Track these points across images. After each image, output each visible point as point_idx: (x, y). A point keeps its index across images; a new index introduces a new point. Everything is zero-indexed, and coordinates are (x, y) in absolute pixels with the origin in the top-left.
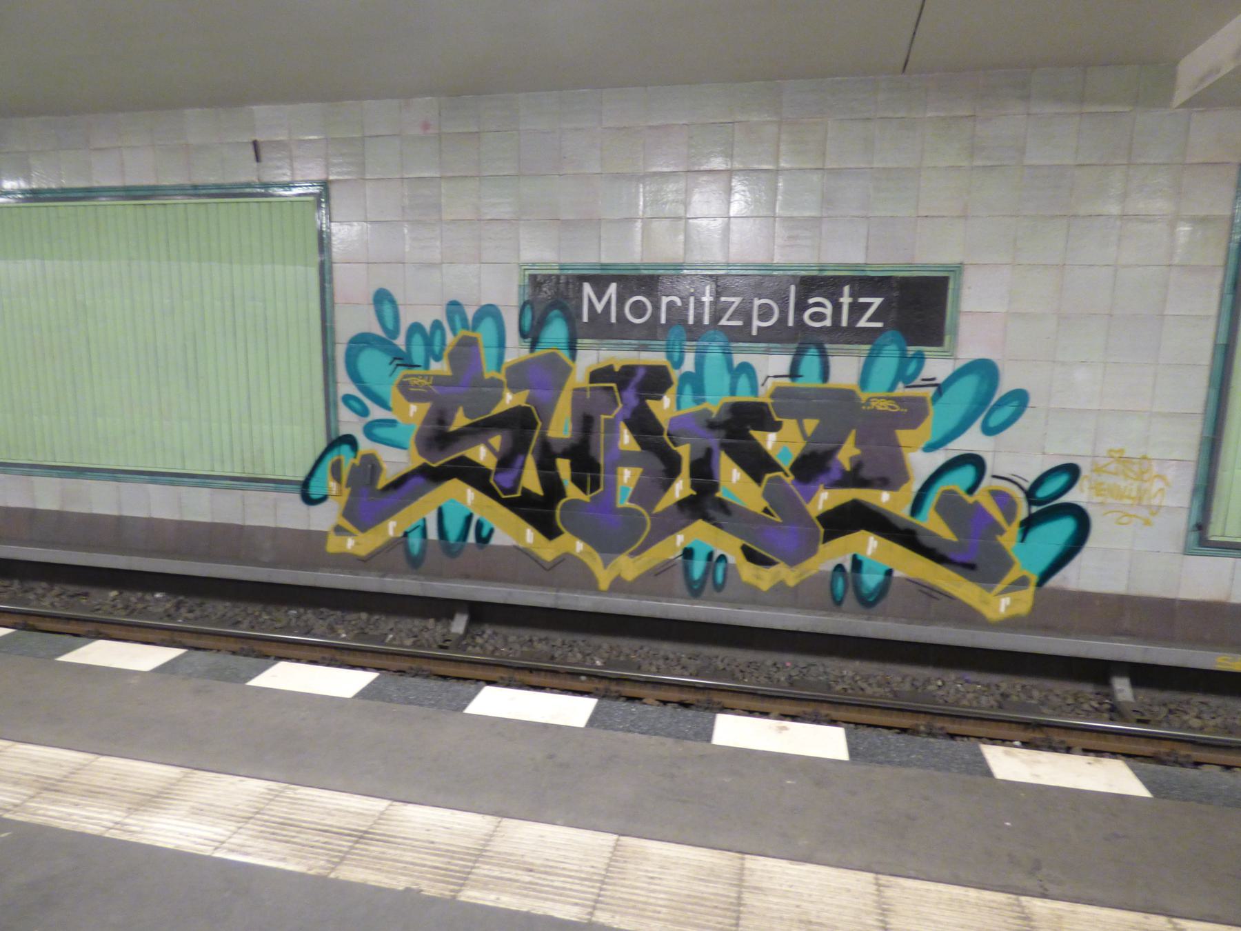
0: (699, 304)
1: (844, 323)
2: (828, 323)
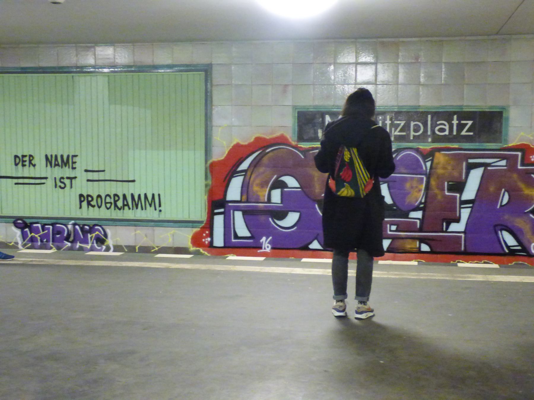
1: (455, 133)
2: (447, 133)
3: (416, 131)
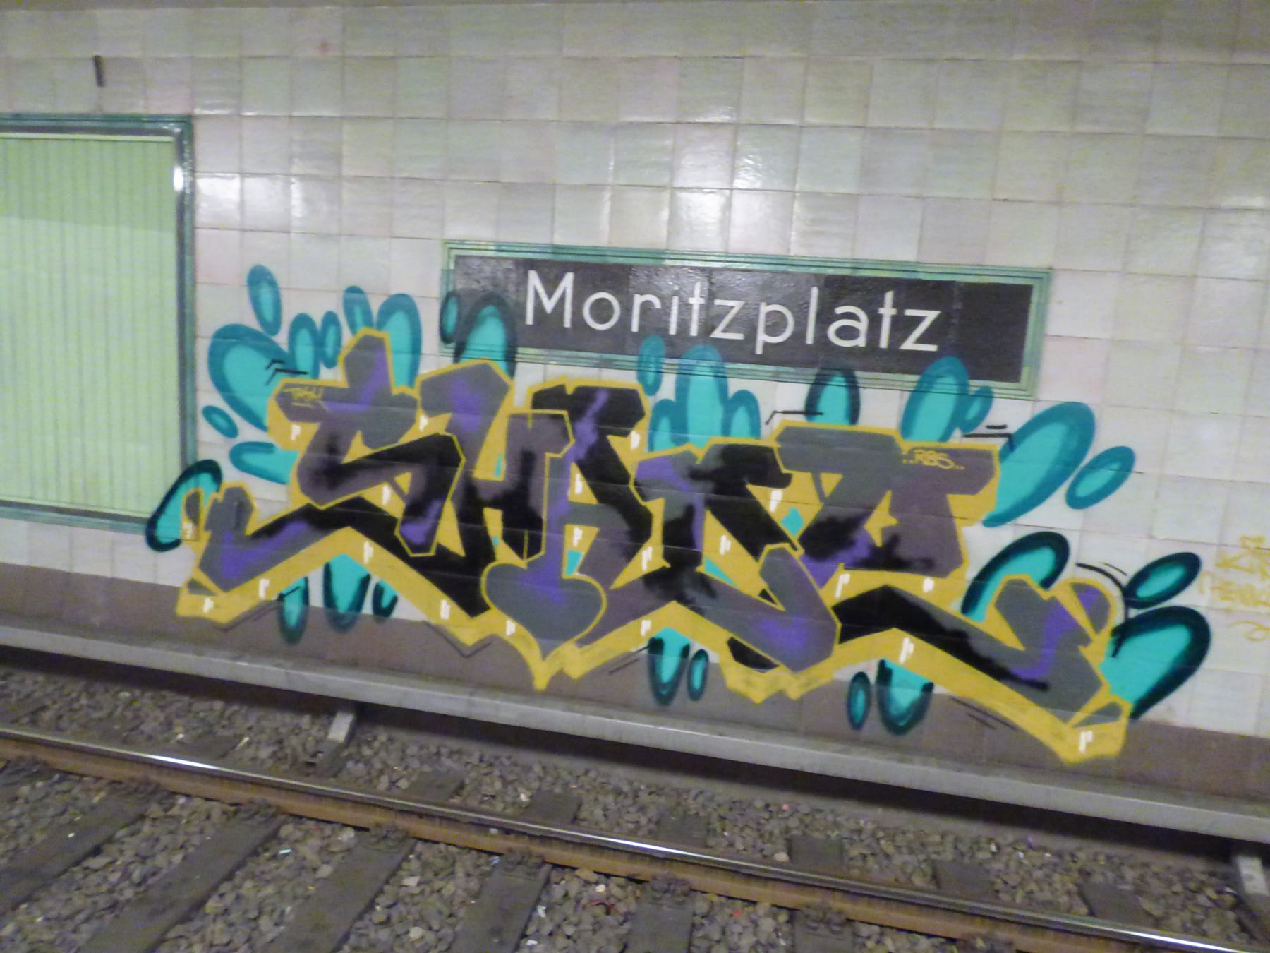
0: (685, 307)
1: (884, 343)
2: (861, 342)
3: (843, 332)
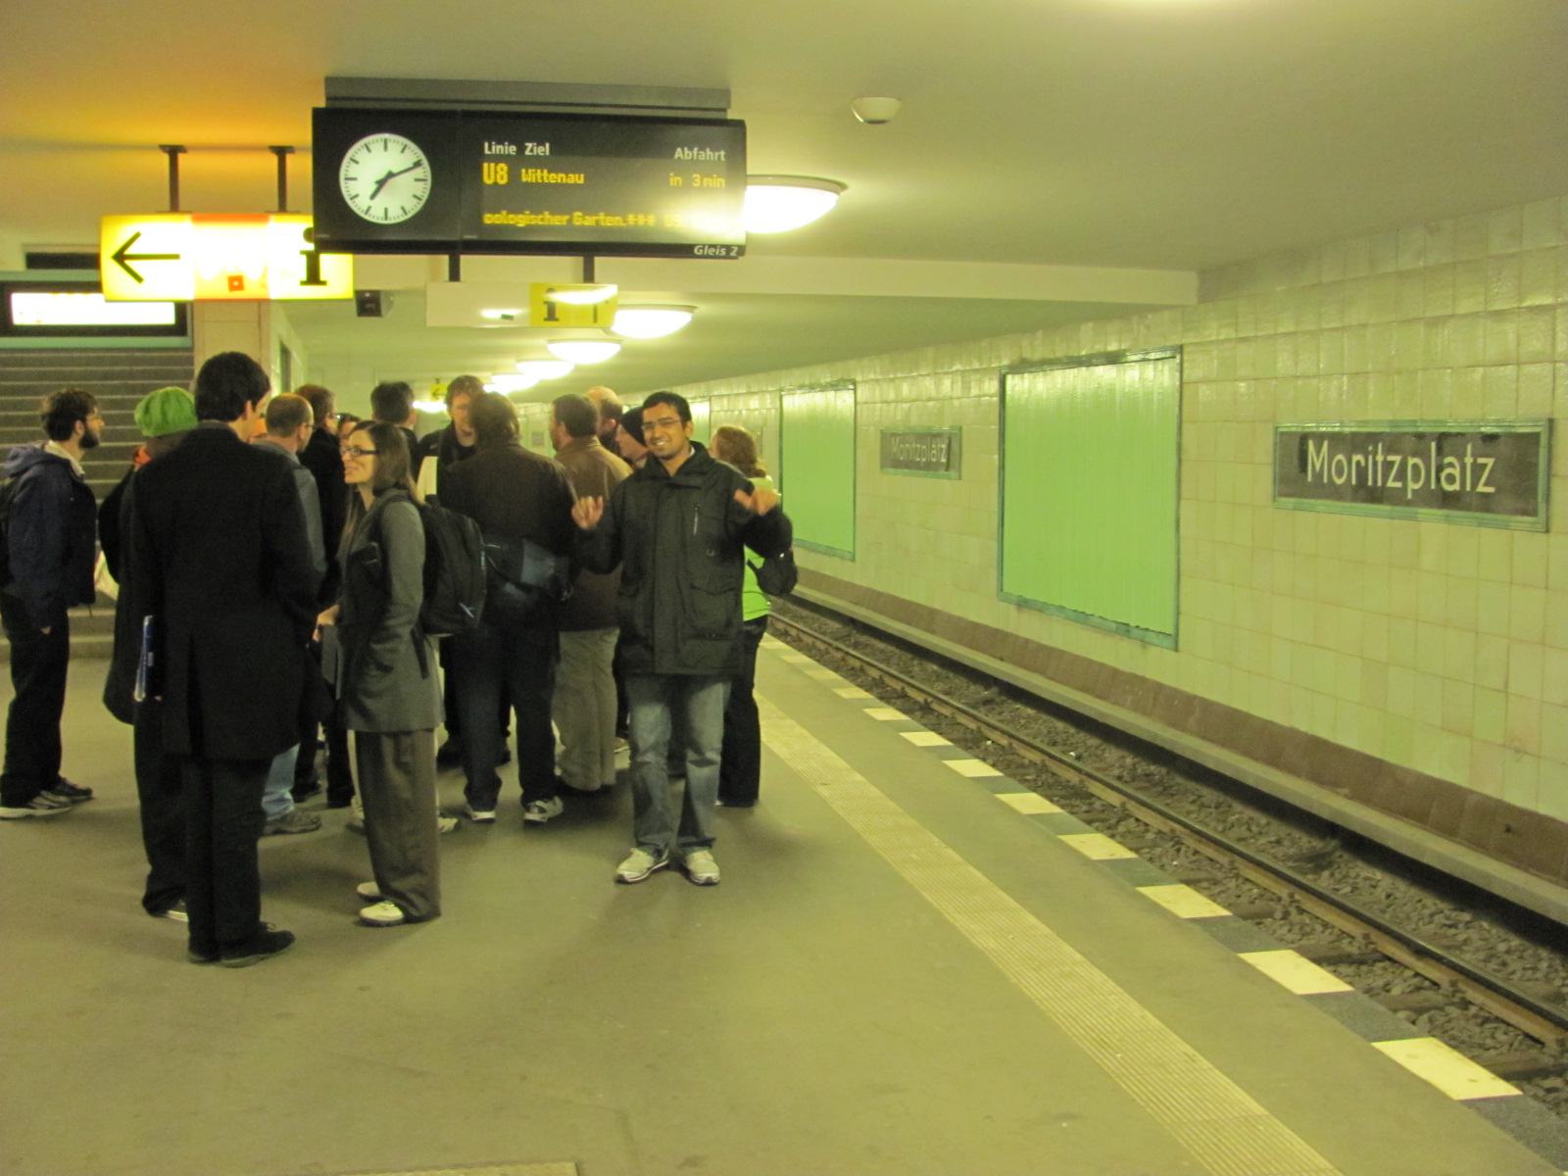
0: (1375, 463)
